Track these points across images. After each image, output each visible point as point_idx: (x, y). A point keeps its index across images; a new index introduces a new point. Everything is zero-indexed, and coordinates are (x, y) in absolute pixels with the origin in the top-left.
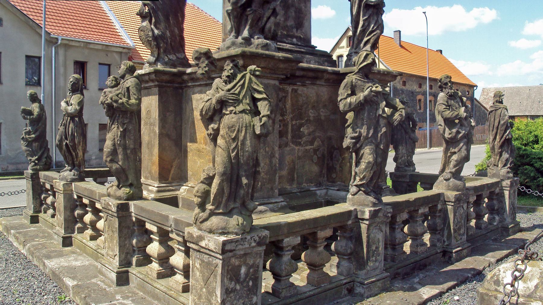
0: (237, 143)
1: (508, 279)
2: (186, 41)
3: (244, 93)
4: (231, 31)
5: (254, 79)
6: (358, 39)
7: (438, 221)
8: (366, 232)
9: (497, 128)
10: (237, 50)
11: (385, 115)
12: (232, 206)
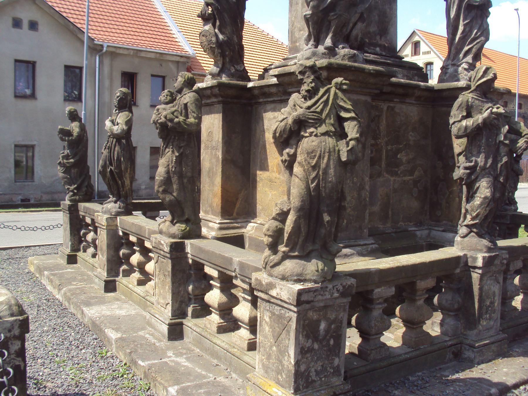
0: (318, 172)
3: (327, 112)
5: (340, 94)
6: (456, 48)
12: (311, 248)
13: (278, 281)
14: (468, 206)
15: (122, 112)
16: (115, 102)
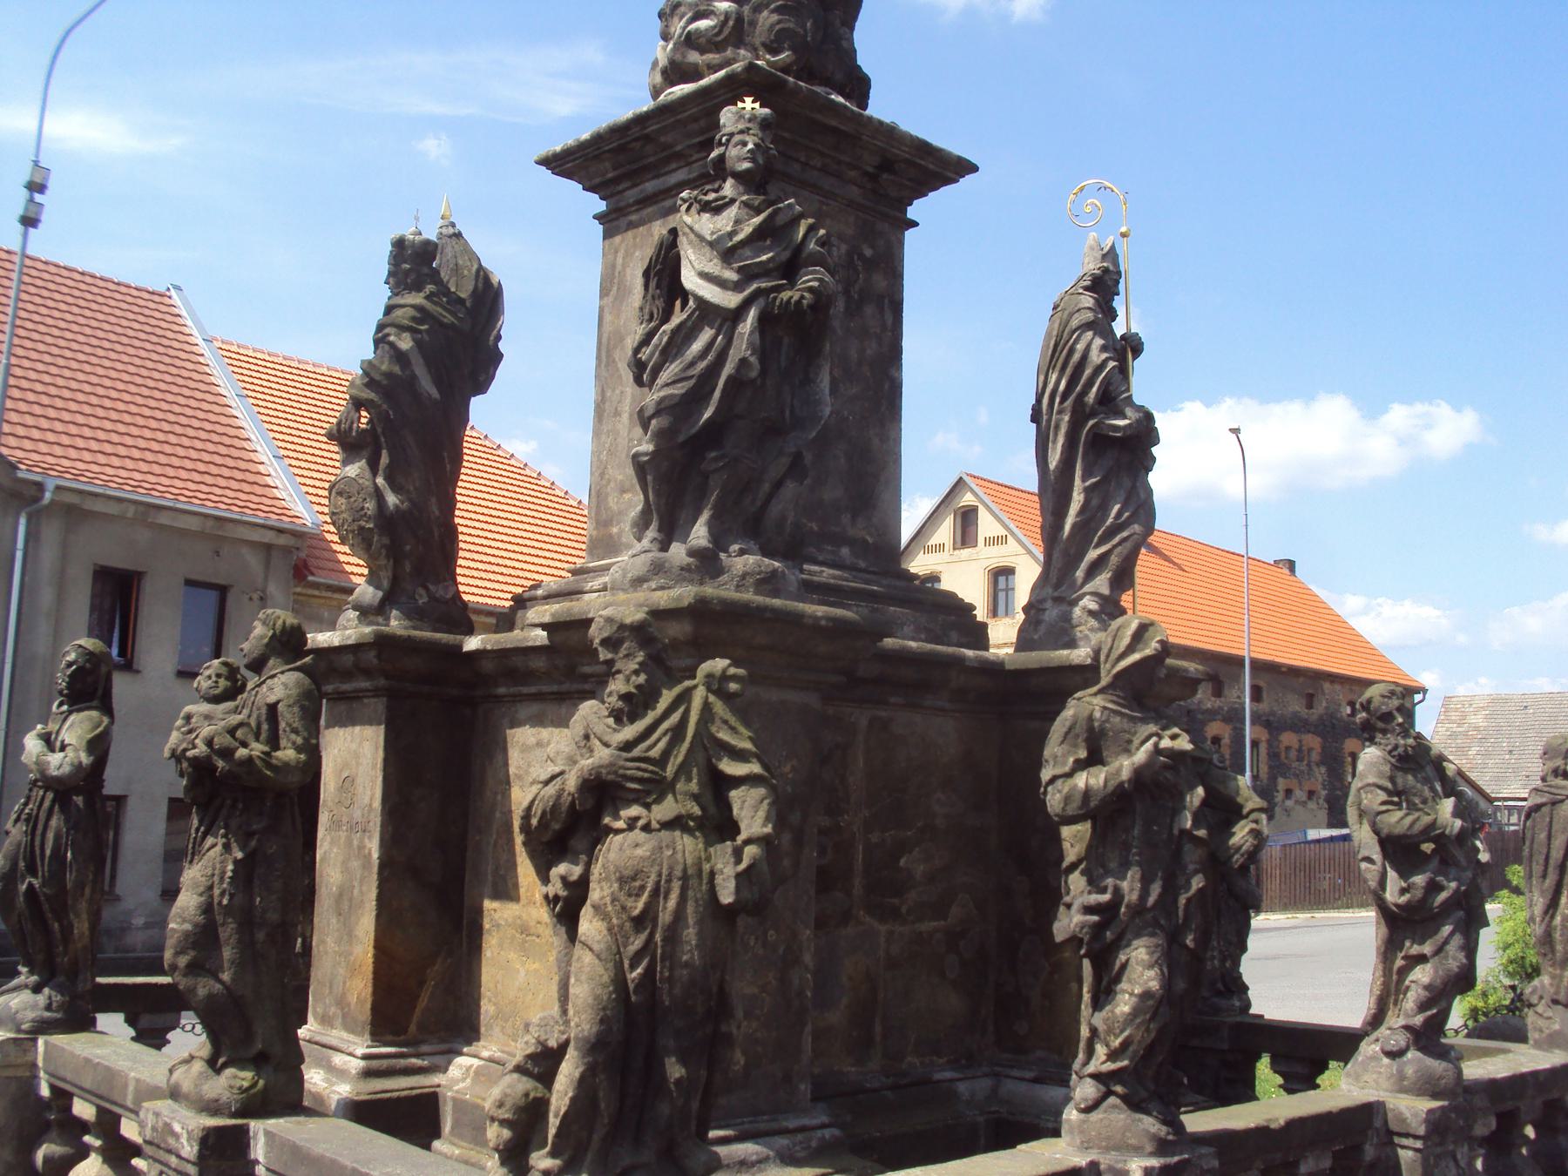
0: (652, 935)
3: (680, 759)
5: (719, 707)
10: (676, 592)
12: (627, 1161)
14: (1099, 1020)
15: (79, 710)
16: (62, 682)
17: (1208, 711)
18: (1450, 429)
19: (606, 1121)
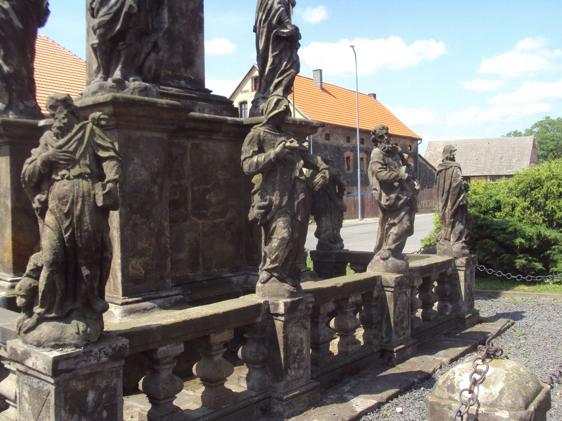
0: (72, 220)
1: (466, 383)
2: (37, 85)
3: (82, 151)
4: (98, 71)
5: (97, 130)
6: (266, 81)
7: (374, 311)
8: (281, 331)
9: (448, 192)
10: (106, 95)
11: (303, 178)
12: (70, 308)
13: (34, 349)
17: (345, 147)
18: (434, 49)
19: (60, 292)
